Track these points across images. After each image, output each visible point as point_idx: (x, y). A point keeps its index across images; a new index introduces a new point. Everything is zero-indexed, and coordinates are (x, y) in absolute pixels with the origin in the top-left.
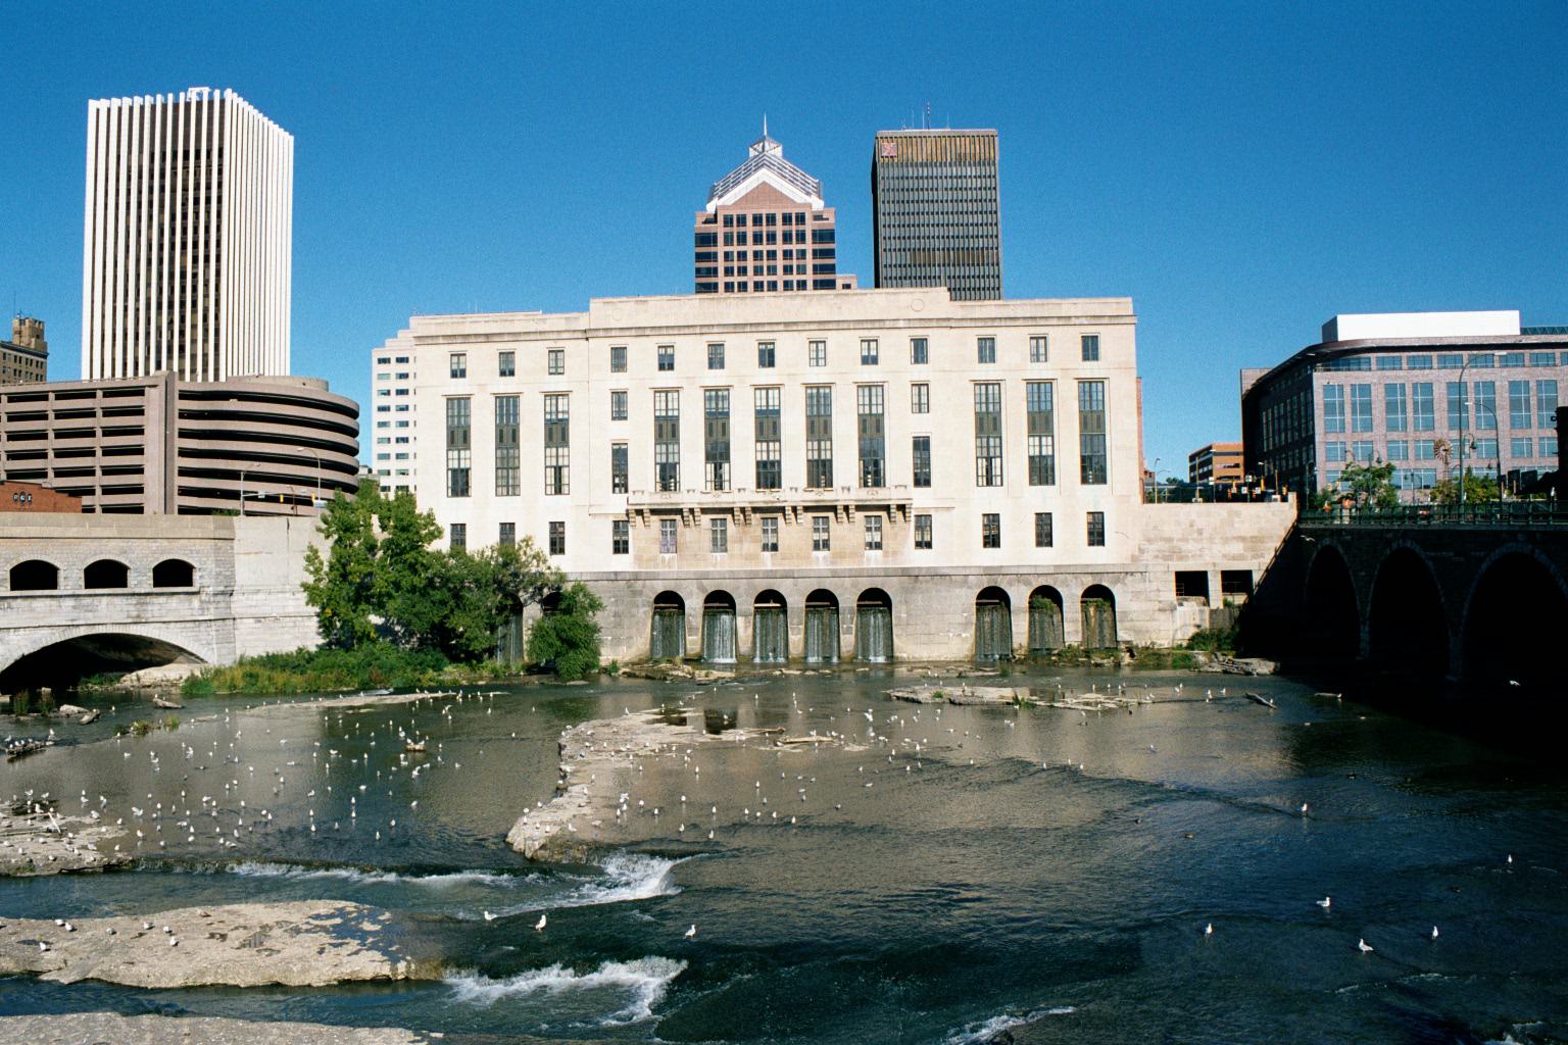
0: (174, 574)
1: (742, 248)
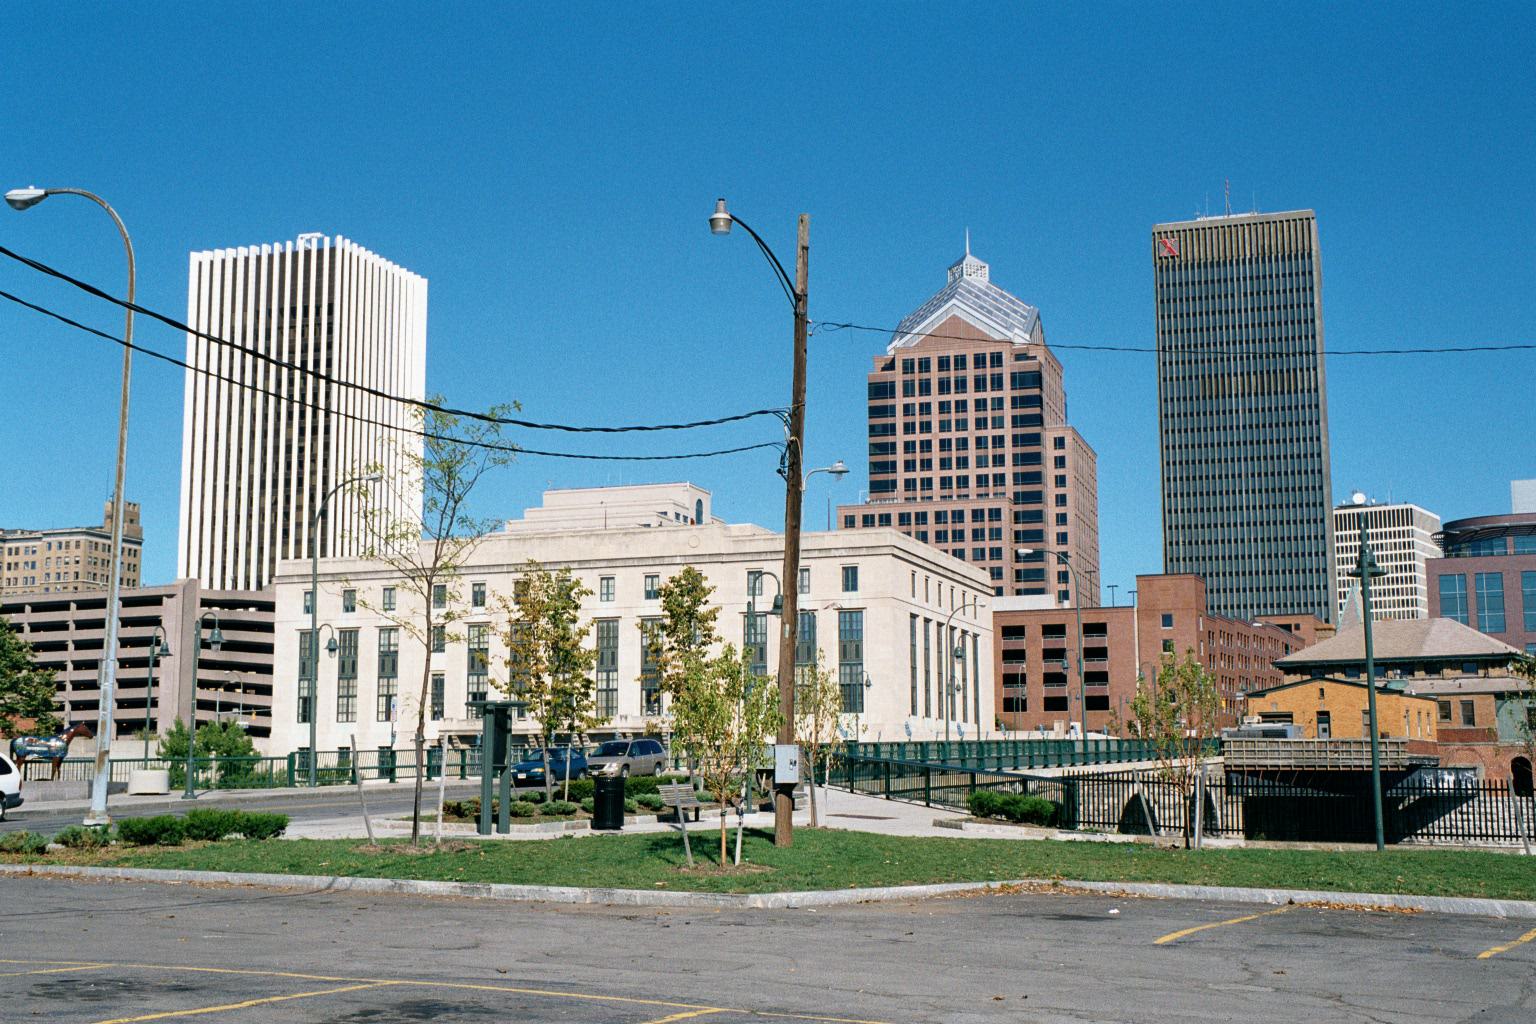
1: (925, 399)
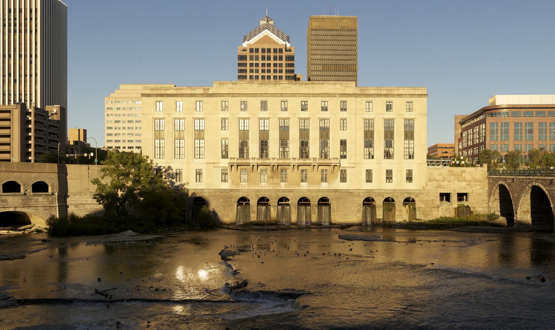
1: (269, 62)
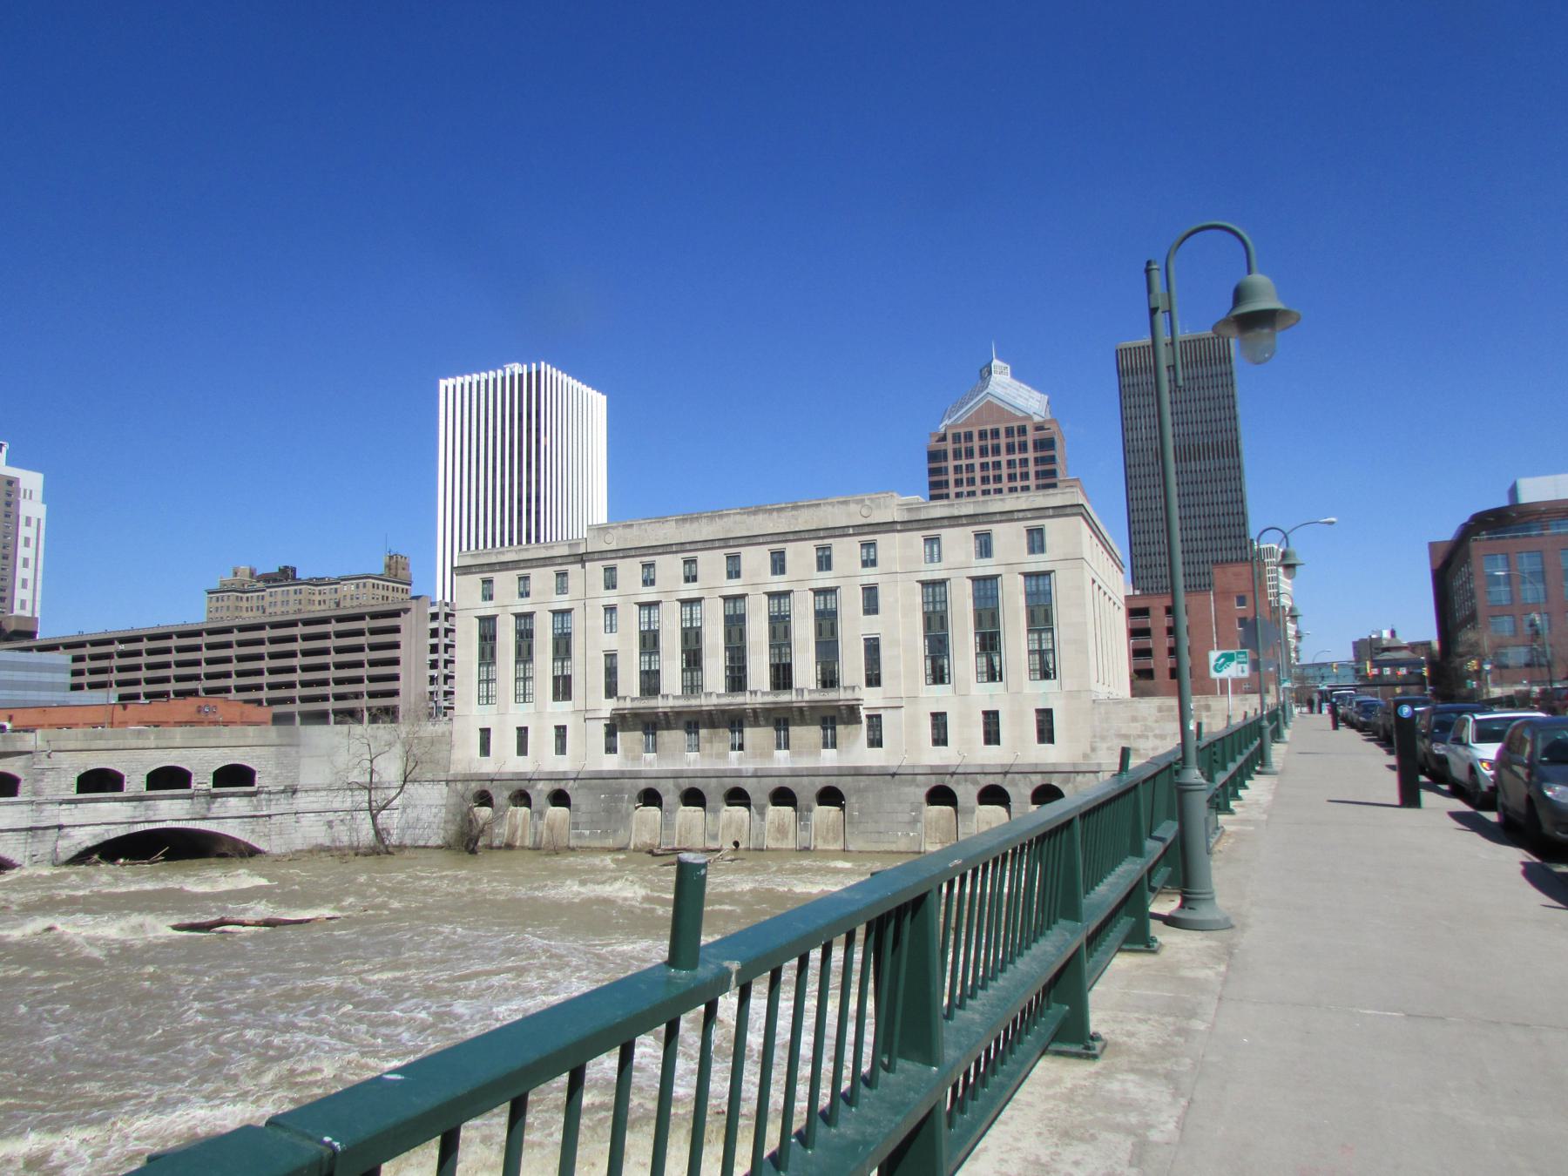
0: (234, 777)
1: (996, 459)
